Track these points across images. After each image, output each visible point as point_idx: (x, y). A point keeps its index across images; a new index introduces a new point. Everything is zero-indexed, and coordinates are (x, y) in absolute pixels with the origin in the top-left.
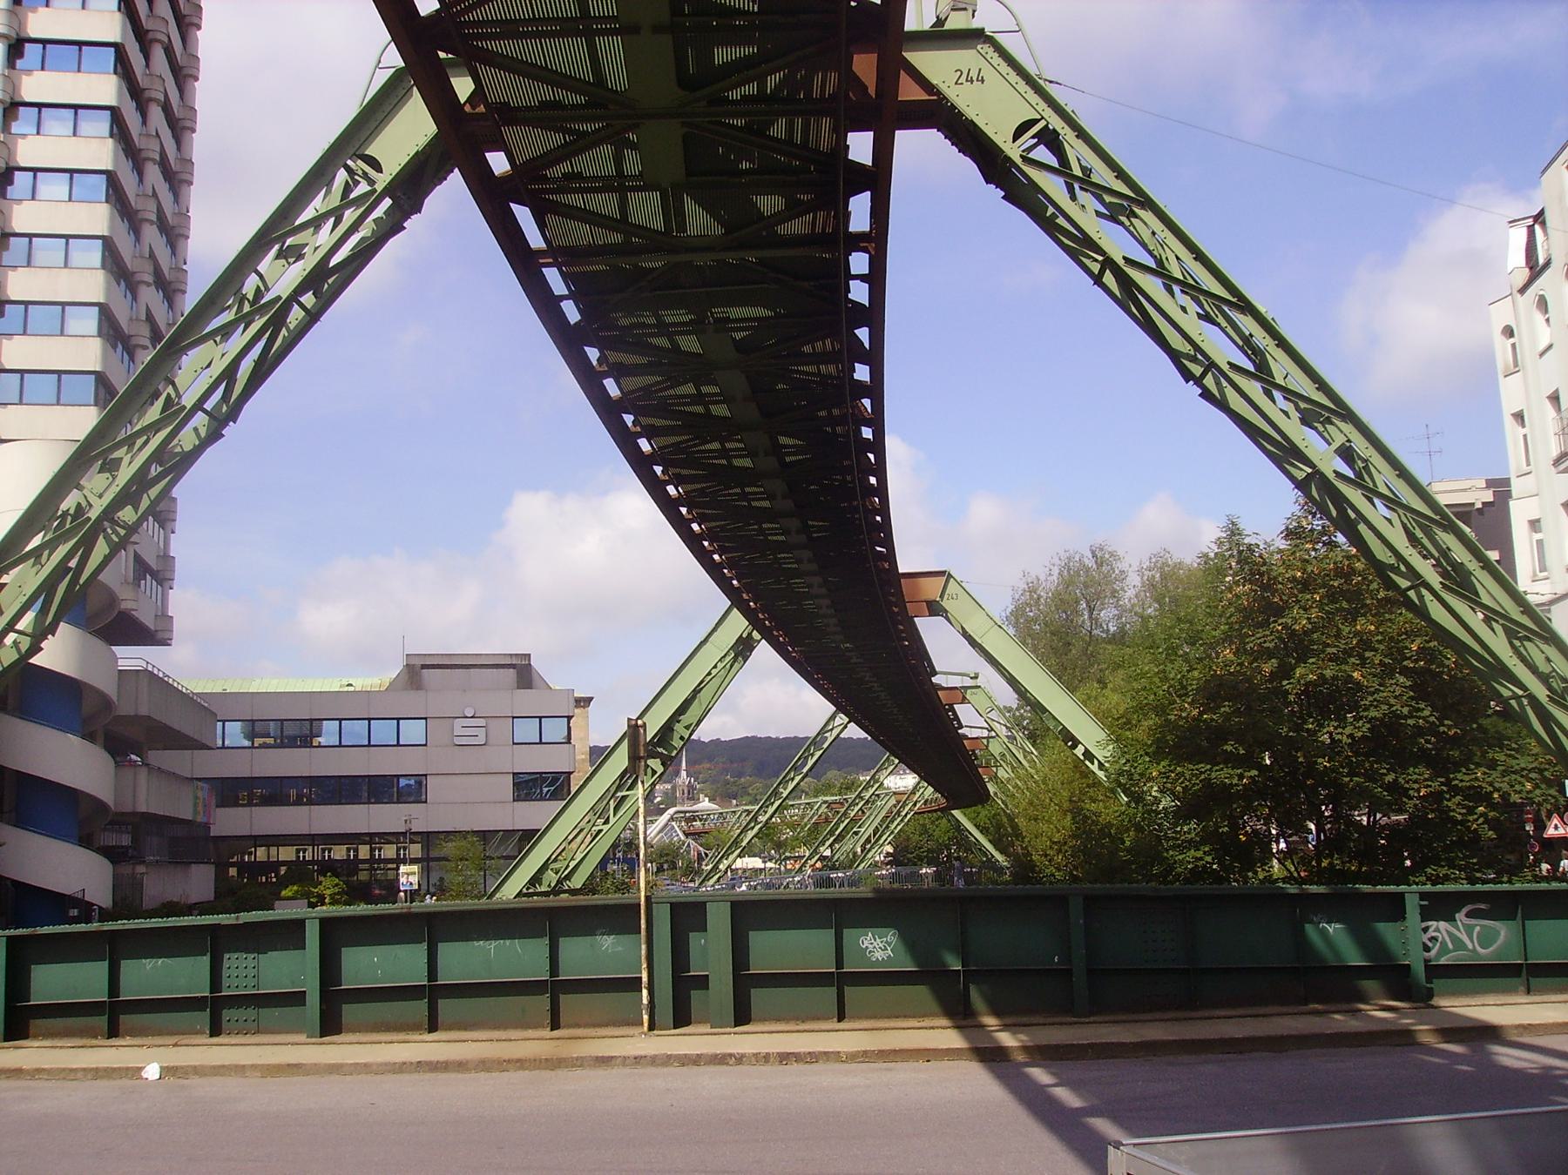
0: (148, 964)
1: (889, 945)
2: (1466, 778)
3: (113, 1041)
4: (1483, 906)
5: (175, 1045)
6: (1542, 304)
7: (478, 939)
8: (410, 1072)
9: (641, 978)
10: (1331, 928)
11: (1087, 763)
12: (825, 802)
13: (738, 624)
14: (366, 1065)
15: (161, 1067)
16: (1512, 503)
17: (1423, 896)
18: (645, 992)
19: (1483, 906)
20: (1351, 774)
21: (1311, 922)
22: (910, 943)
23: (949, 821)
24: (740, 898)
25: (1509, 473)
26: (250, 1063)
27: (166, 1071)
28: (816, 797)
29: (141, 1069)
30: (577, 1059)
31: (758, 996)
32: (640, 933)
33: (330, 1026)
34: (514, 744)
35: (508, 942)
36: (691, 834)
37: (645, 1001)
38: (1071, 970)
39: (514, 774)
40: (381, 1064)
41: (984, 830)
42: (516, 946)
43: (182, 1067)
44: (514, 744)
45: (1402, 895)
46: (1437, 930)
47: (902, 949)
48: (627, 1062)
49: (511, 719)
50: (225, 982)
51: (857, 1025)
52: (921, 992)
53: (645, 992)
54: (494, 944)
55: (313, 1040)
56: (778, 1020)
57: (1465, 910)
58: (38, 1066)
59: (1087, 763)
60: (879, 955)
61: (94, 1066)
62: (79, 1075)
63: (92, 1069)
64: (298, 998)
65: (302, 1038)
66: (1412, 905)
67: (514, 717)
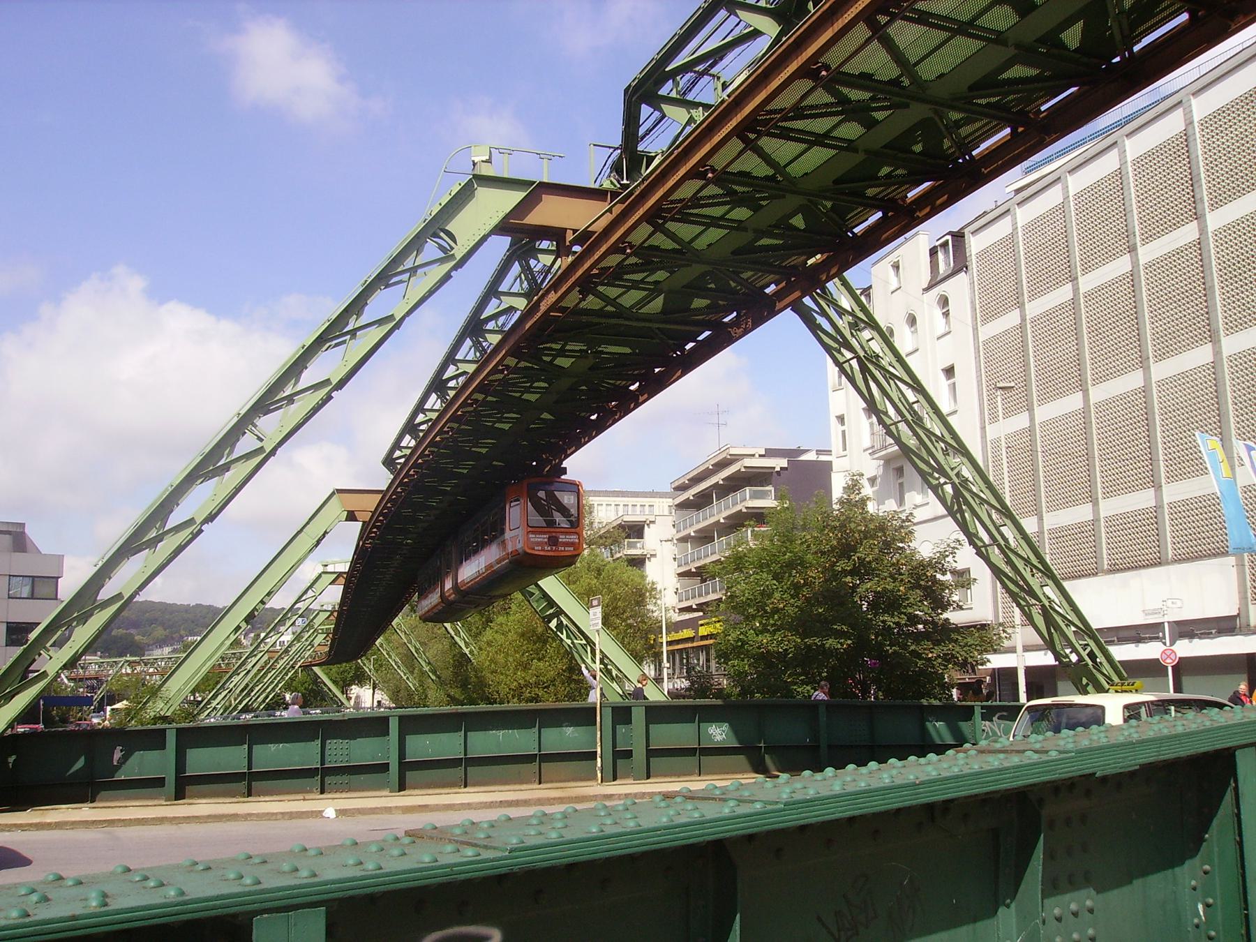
0: (273, 747)
1: (724, 731)
2: (945, 649)
3: (250, 799)
4: (1005, 714)
5: (304, 800)
6: (944, 301)
7: (492, 730)
8: (496, 808)
9: (596, 752)
10: (937, 724)
11: (559, 633)
12: (127, 661)
13: (372, 502)
14: (468, 804)
15: (336, 810)
16: (833, 475)
17: (983, 707)
18: (599, 760)
19: (1005, 714)
20: (891, 645)
21: (929, 721)
22: (735, 730)
23: (309, 675)
24: (652, 704)
25: (831, 447)
26: (395, 805)
27: (341, 812)
28: (121, 656)
29: (321, 812)
30: (593, 796)
31: (410, 775)
32: (596, 724)
33: (179, 795)
34: (9, 598)
35: (510, 731)
36: (72, 679)
37: (599, 764)
38: (819, 746)
39: (7, 623)
40: (478, 803)
41: (335, 682)
42: (515, 734)
43: (350, 810)
44: (9, 598)
45: (973, 706)
46: (985, 726)
47: (731, 734)
48: (622, 797)
49: (8, 577)
50: (328, 759)
51: (549, 785)
52: (741, 758)
53: (599, 760)
54: (502, 732)
55: (393, 794)
56: (665, 776)
57: (997, 716)
58: (249, 812)
59: (559, 633)
60: (719, 738)
61: (288, 811)
62: (279, 817)
63: (288, 813)
64: (384, 768)
65: (386, 793)
66: (978, 711)
67: (10, 576)
